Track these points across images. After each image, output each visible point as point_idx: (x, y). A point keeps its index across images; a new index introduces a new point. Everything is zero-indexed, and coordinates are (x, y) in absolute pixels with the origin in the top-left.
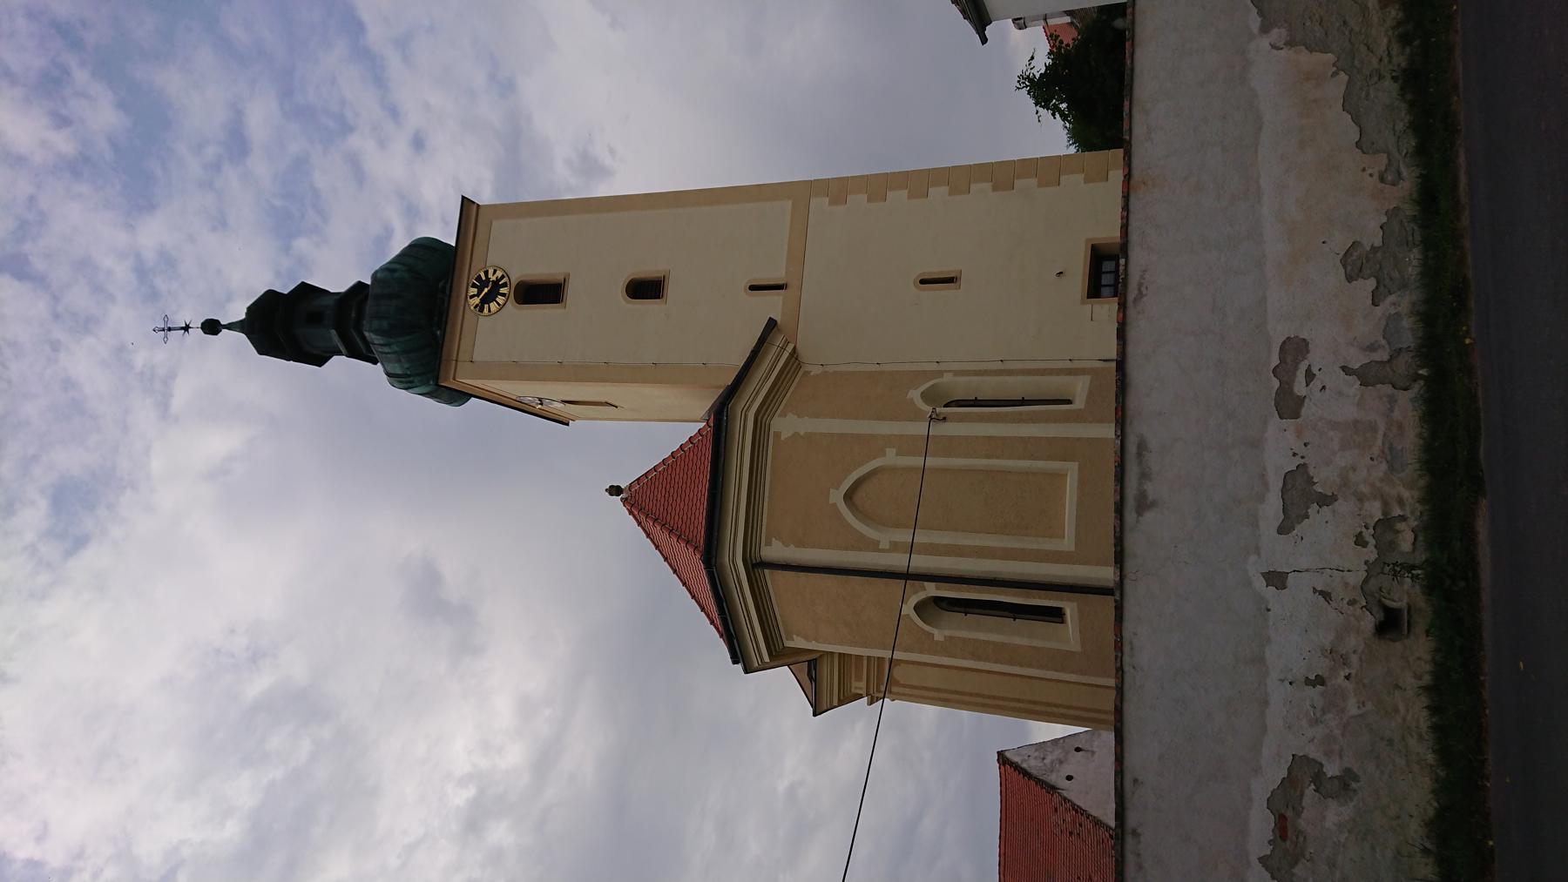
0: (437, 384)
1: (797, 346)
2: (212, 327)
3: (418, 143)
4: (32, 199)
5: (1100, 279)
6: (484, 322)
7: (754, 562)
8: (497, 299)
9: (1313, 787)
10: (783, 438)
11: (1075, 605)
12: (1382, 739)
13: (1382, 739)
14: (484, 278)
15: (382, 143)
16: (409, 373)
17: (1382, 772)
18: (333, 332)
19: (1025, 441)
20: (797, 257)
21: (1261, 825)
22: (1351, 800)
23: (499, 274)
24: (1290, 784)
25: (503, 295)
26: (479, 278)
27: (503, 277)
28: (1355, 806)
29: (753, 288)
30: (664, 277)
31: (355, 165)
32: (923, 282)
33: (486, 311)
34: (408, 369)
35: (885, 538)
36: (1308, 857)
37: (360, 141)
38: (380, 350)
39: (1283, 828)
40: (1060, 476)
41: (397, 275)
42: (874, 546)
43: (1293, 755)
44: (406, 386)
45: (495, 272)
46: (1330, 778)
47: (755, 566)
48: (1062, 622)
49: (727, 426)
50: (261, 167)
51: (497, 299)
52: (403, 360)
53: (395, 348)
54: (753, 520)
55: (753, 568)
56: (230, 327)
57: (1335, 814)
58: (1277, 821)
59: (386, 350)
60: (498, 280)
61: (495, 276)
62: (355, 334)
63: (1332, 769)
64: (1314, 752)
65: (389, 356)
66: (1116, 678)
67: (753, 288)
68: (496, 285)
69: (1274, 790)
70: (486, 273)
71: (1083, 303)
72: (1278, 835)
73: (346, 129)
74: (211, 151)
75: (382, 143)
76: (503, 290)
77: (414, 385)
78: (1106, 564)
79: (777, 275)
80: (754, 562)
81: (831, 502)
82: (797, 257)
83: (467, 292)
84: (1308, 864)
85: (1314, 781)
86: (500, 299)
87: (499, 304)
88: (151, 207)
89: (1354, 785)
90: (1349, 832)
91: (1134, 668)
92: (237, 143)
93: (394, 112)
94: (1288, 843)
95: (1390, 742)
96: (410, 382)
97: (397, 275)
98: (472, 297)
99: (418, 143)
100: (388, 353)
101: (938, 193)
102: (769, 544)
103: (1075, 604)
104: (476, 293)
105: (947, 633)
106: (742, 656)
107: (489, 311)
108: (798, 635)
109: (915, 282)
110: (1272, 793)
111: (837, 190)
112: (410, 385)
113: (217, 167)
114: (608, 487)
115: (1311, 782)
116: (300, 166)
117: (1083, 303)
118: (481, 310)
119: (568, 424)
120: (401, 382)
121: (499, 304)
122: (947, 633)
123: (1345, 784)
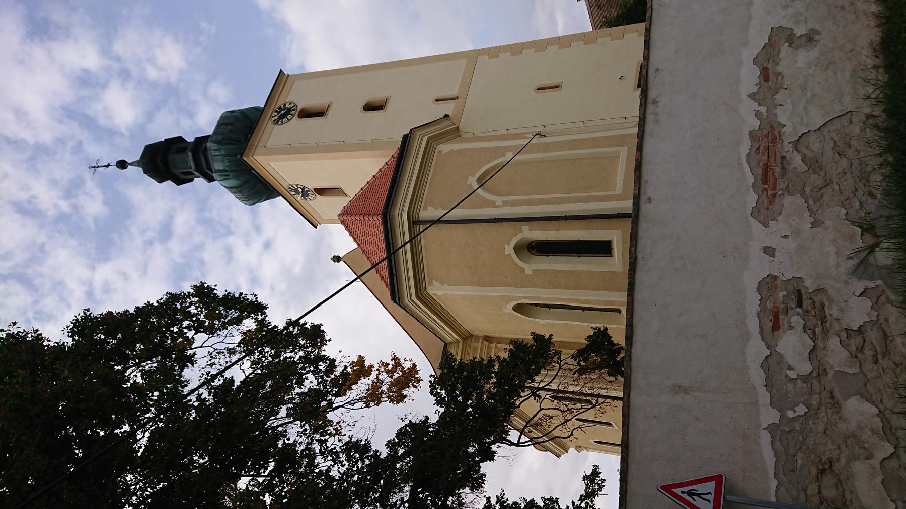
0: (241, 158)
1: (460, 126)
2: (122, 165)
3: (267, 245)
4: (43, 244)
7: (414, 220)
9: (787, 44)
10: (443, 153)
11: (619, 231)
12: (836, 7)
13: (836, 7)
15: (247, 243)
16: (227, 169)
17: (838, 26)
18: (190, 154)
19: (593, 139)
20: (467, 84)
21: (750, 77)
22: (816, 46)
23: (292, 105)
24: (770, 49)
25: (292, 114)
27: (294, 106)
28: (818, 50)
30: (386, 100)
31: (229, 252)
32: (539, 89)
33: (280, 122)
34: (227, 166)
35: (499, 200)
36: (785, 86)
37: (235, 241)
38: (214, 154)
39: (765, 75)
40: (614, 158)
41: (234, 114)
42: (493, 204)
43: (772, 28)
44: (224, 178)
46: (799, 37)
47: (414, 222)
48: (611, 256)
49: (409, 139)
50: (175, 246)
52: (226, 161)
53: (223, 152)
54: (417, 197)
55: (413, 224)
56: (131, 164)
57: (804, 57)
58: (761, 71)
59: (217, 153)
62: (203, 159)
63: (800, 31)
64: (785, 23)
65: (218, 157)
68: (289, 109)
69: (758, 53)
71: (634, 90)
72: (762, 80)
73: (229, 232)
74: (150, 235)
75: (247, 243)
76: (292, 112)
77: (228, 177)
79: (454, 93)
80: (414, 220)
81: (468, 183)
82: (467, 84)
84: (786, 91)
85: (787, 41)
86: (289, 117)
87: (288, 119)
88: (107, 259)
89: (817, 37)
90: (816, 66)
91: (660, 5)
92: (166, 232)
93: (258, 229)
94: (770, 83)
95: (843, 8)
96: (227, 176)
97: (234, 114)
99: (267, 245)
100: (218, 155)
101: (552, 49)
102: (425, 209)
103: (620, 231)
105: (535, 267)
106: (398, 295)
107: (282, 122)
108: (436, 281)
109: (534, 90)
110: (757, 55)
111: (493, 53)
112: (226, 178)
113: (150, 243)
114: (332, 257)
115: (785, 42)
116: (200, 247)
117: (634, 90)
118: (277, 122)
120: (221, 175)
122: (535, 267)
123: (810, 38)
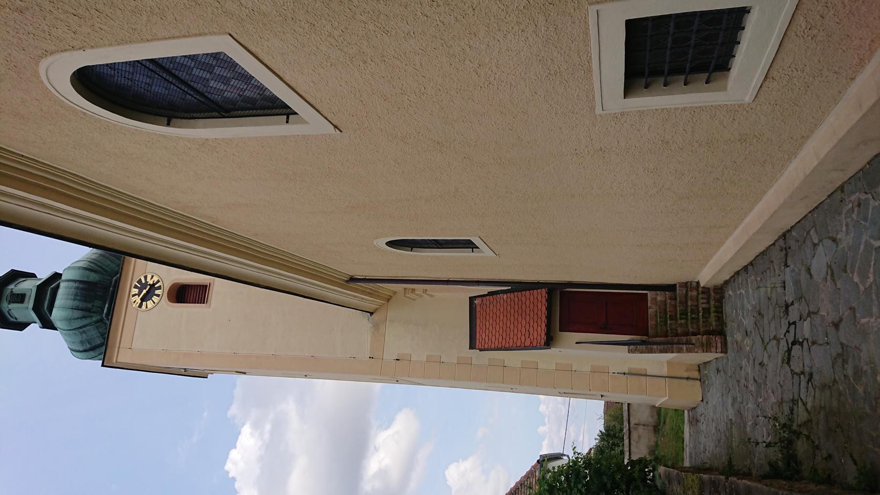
5: (179, 77)
6: (142, 314)
8: (153, 299)
14: (143, 281)
23: (155, 279)
25: (158, 295)
26: (140, 281)
27: (158, 281)
29: (576, 343)
30: (210, 284)
33: (144, 307)
45: (152, 277)
51: (153, 299)
60: (154, 284)
61: (152, 280)
66: (690, 468)
67: (576, 343)
70: (146, 277)
76: (157, 292)
78: (690, 462)
83: (130, 291)
86: (155, 299)
87: (154, 303)
98: (134, 296)
104: (137, 293)
107: (147, 307)
119: (207, 378)
121: (154, 303)
